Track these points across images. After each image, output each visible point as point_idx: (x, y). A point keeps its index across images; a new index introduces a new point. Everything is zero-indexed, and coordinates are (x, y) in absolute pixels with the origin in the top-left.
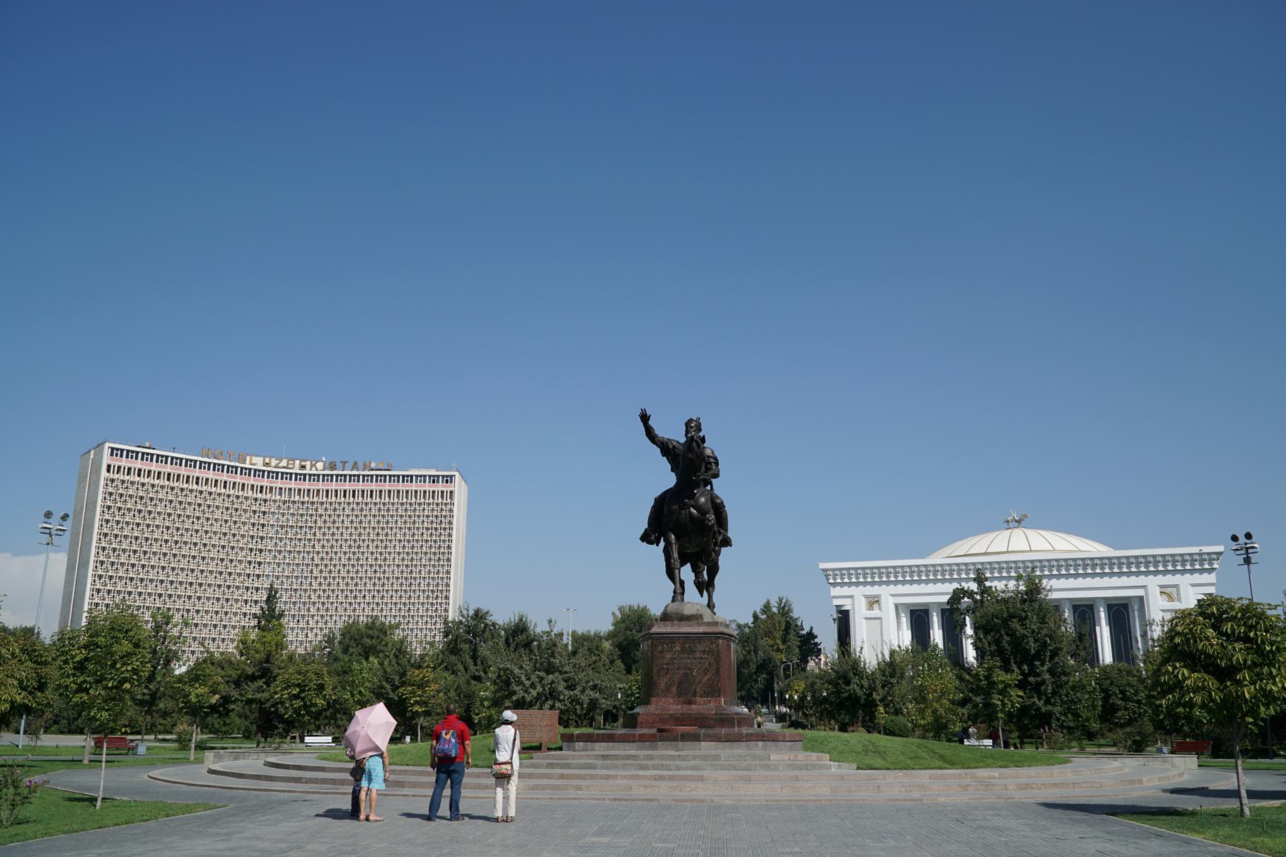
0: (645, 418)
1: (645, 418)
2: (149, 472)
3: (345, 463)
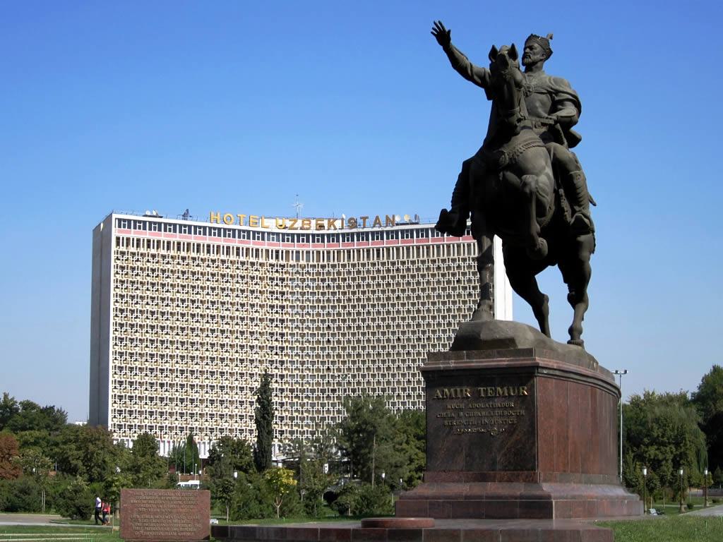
0: (443, 37)
1: (443, 37)
2: (159, 242)
3: (364, 219)
